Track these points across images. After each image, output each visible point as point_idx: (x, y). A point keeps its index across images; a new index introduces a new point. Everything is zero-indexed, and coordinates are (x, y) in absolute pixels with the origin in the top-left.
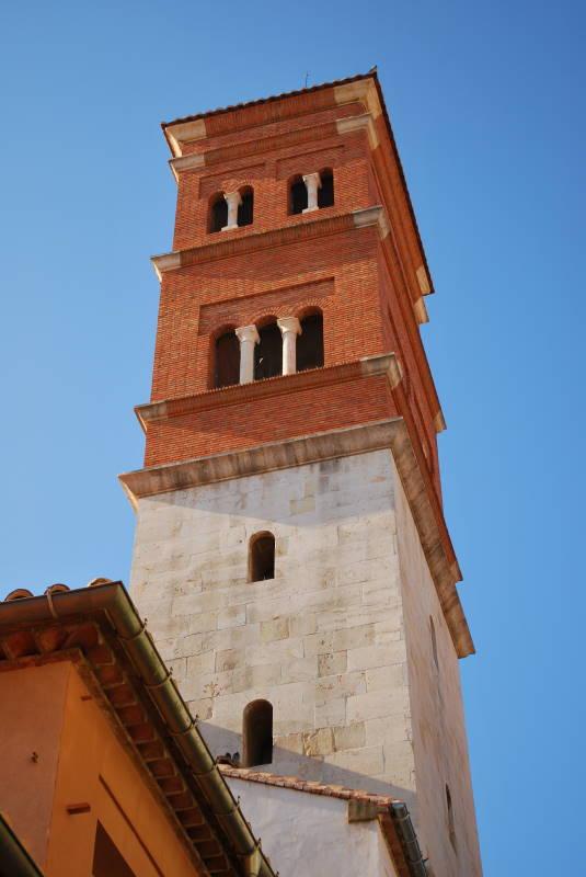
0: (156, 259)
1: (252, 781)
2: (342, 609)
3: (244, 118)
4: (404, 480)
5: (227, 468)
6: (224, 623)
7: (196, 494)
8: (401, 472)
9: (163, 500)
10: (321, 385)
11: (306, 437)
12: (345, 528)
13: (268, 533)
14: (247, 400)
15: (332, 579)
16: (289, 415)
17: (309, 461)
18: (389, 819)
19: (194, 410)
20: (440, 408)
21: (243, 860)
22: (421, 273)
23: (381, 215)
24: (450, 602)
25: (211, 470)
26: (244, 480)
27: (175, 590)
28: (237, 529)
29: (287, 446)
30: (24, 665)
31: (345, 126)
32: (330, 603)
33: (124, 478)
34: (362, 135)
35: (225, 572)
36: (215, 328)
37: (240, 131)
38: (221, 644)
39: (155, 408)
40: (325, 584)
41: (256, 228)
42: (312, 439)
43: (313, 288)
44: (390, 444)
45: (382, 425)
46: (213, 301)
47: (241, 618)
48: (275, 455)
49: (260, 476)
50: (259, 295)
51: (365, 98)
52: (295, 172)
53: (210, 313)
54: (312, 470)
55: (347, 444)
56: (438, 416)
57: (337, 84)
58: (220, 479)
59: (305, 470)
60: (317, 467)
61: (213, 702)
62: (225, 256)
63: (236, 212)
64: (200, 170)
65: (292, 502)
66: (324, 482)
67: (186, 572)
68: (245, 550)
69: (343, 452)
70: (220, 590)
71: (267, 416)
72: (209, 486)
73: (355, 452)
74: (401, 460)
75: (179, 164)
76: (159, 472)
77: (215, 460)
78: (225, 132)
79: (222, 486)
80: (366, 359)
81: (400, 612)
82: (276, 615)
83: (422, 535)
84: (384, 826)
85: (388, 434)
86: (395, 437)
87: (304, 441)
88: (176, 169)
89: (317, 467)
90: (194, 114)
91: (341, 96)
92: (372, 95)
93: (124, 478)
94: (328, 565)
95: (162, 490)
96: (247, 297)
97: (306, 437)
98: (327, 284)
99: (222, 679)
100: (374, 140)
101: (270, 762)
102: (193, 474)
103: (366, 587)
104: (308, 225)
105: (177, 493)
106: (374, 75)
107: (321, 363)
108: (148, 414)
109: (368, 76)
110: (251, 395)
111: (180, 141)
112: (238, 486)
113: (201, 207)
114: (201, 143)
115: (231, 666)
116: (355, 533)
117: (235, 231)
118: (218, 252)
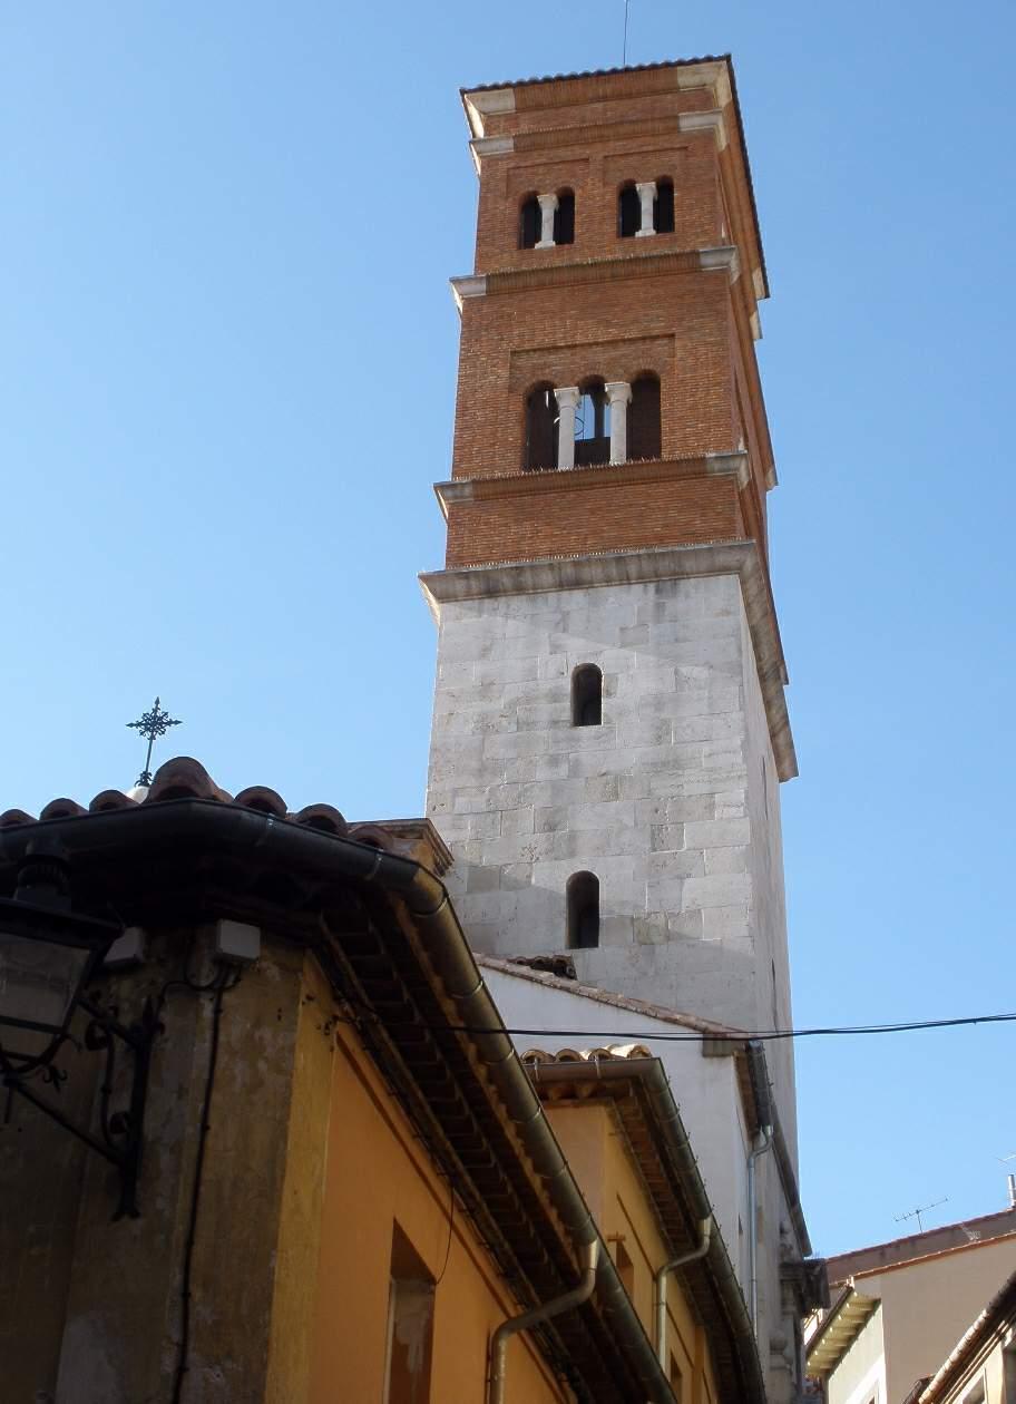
0: (456, 281)
1: (601, 1002)
2: (680, 772)
3: (564, 93)
4: (748, 606)
5: (547, 578)
6: (542, 774)
7: (508, 606)
8: (746, 599)
9: (470, 609)
10: (656, 479)
11: (642, 552)
12: (684, 670)
13: (593, 666)
14: (566, 489)
15: (668, 733)
16: (618, 515)
17: (642, 579)
18: (744, 1055)
19: (504, 494)
20: (773, 462)
21: (698, 1223)
22: (757, 275)
23: (734, 257)
24: (781, 724)
25: (528, 578)
26: (565, 594)
27: (486, 727)
28: (559, 656)
29: (619, 560)
30: (563, 1106)
31: (690, 122)
32: (664, 764)
33: (425, 578)
34: (709, 136)
35: (544, 711)
36: (527, 384)
37: (557, 108)
38: (541, 799)
39: (459, 488)
40: (659, 739)
41: (579, 254)
42: (649, 555)
43: (648, 344)
44: (739, 570)
45: (730, 547)
46: (527, 346)
47: (564, 770)
48: (603, 569)
49: (585, 590)
50: (582, 345)
51: (714, 84)
52: (628, 176)
53: (522, 361)
54: (645, 591)
55: (689, 565)
56: (770, 474)
57: (681, 63)
58: (535, 590)
59: (637, 589)
60: (652, 587)
61: (532, 868)
62: (541, 286)
63: (552, 222)
64: (508, 157)
65: (622, 629)
66: (660, 607)
67: (500, 704)
68: (567, 685)
69: (683, 574)
70: (538, 733)
71: (592, 512)
72: (524, 597)
73: (698, 574)
74: (748, 586)
75: (482, 147)
76: (466, 576)
77: (533, 568)
78: (539, 107)
79: (540, 599)
80: (713, 455)
81: (744, 784)
82: (603, 771)
83: (759, 659)
84: (738, 1059)
85: (738, 557)
86: (744, 563)
87: (639, 556)
88: (478, 153)
89: (652, 587)
90: (501, 82)
91: (685, 79)
92: (723, 80)
93: (425, 578)
94: (663, 716)
95: (469, 596)
96: (569, 347)
97: (642, 552)
98: (665, 341)
99: (540, 841)
100: (723, 140)
101: (596, 945)
102: (507, 581)
103: (706, 749)
104: (645, 259)
105: (486, 601)
106: (728, 58)
107: (658, 454)
108: (449, 493)
109: (720, 59)
110: (569, 483)
111: (481, 112)
112: (559, 600)
113: (510, 210)
114: (508, 117)
115: (551, 827)
116: (695, 679)
117: (549, 251)
118: (533, 281)
